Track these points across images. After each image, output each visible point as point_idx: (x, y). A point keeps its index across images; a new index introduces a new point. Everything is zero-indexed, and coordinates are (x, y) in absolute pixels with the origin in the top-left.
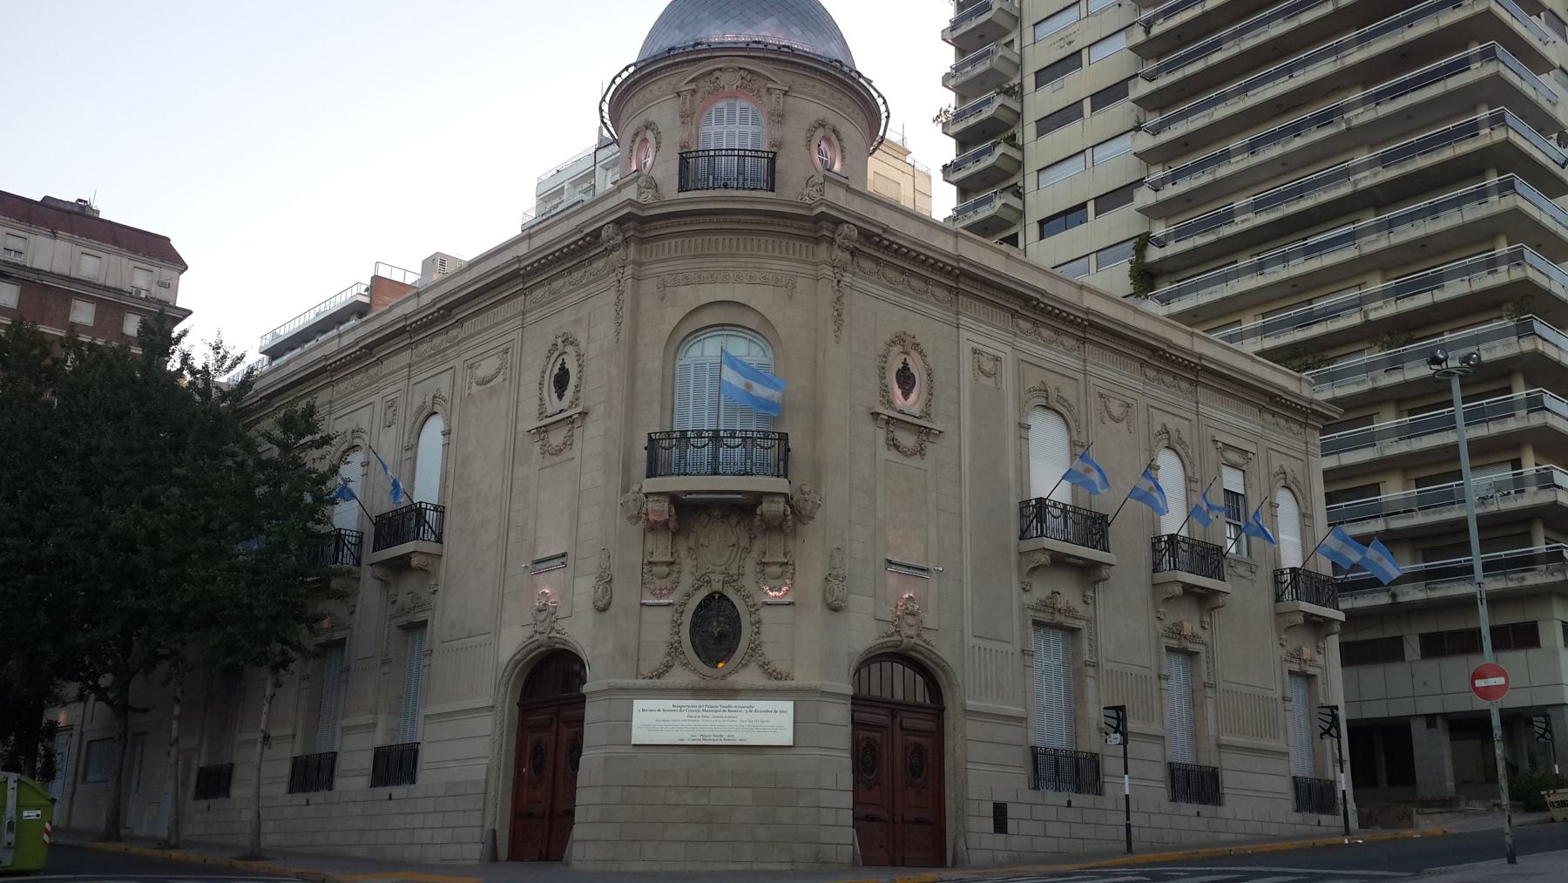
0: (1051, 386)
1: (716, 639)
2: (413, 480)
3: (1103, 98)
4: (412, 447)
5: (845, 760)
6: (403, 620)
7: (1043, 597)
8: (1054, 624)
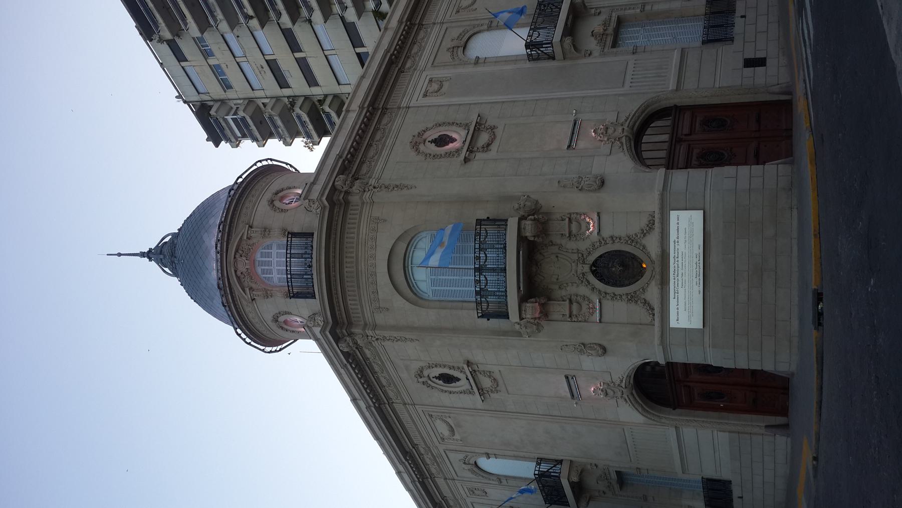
0: (450, 44)
1: (625, 269)
2: (520, 478)
3: (294, 45)
4: (499, 479)
5: (714, 173)
6: (617, 487)
7: (595, 42)
8: (614, 35)
